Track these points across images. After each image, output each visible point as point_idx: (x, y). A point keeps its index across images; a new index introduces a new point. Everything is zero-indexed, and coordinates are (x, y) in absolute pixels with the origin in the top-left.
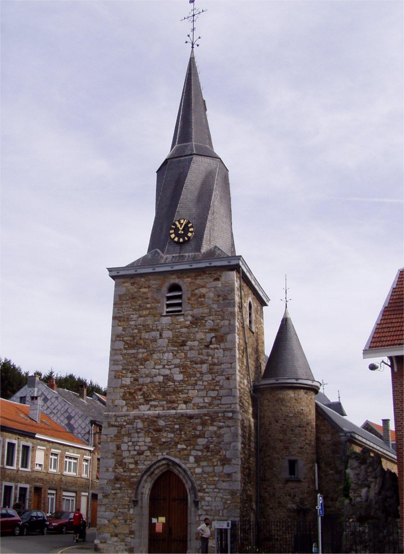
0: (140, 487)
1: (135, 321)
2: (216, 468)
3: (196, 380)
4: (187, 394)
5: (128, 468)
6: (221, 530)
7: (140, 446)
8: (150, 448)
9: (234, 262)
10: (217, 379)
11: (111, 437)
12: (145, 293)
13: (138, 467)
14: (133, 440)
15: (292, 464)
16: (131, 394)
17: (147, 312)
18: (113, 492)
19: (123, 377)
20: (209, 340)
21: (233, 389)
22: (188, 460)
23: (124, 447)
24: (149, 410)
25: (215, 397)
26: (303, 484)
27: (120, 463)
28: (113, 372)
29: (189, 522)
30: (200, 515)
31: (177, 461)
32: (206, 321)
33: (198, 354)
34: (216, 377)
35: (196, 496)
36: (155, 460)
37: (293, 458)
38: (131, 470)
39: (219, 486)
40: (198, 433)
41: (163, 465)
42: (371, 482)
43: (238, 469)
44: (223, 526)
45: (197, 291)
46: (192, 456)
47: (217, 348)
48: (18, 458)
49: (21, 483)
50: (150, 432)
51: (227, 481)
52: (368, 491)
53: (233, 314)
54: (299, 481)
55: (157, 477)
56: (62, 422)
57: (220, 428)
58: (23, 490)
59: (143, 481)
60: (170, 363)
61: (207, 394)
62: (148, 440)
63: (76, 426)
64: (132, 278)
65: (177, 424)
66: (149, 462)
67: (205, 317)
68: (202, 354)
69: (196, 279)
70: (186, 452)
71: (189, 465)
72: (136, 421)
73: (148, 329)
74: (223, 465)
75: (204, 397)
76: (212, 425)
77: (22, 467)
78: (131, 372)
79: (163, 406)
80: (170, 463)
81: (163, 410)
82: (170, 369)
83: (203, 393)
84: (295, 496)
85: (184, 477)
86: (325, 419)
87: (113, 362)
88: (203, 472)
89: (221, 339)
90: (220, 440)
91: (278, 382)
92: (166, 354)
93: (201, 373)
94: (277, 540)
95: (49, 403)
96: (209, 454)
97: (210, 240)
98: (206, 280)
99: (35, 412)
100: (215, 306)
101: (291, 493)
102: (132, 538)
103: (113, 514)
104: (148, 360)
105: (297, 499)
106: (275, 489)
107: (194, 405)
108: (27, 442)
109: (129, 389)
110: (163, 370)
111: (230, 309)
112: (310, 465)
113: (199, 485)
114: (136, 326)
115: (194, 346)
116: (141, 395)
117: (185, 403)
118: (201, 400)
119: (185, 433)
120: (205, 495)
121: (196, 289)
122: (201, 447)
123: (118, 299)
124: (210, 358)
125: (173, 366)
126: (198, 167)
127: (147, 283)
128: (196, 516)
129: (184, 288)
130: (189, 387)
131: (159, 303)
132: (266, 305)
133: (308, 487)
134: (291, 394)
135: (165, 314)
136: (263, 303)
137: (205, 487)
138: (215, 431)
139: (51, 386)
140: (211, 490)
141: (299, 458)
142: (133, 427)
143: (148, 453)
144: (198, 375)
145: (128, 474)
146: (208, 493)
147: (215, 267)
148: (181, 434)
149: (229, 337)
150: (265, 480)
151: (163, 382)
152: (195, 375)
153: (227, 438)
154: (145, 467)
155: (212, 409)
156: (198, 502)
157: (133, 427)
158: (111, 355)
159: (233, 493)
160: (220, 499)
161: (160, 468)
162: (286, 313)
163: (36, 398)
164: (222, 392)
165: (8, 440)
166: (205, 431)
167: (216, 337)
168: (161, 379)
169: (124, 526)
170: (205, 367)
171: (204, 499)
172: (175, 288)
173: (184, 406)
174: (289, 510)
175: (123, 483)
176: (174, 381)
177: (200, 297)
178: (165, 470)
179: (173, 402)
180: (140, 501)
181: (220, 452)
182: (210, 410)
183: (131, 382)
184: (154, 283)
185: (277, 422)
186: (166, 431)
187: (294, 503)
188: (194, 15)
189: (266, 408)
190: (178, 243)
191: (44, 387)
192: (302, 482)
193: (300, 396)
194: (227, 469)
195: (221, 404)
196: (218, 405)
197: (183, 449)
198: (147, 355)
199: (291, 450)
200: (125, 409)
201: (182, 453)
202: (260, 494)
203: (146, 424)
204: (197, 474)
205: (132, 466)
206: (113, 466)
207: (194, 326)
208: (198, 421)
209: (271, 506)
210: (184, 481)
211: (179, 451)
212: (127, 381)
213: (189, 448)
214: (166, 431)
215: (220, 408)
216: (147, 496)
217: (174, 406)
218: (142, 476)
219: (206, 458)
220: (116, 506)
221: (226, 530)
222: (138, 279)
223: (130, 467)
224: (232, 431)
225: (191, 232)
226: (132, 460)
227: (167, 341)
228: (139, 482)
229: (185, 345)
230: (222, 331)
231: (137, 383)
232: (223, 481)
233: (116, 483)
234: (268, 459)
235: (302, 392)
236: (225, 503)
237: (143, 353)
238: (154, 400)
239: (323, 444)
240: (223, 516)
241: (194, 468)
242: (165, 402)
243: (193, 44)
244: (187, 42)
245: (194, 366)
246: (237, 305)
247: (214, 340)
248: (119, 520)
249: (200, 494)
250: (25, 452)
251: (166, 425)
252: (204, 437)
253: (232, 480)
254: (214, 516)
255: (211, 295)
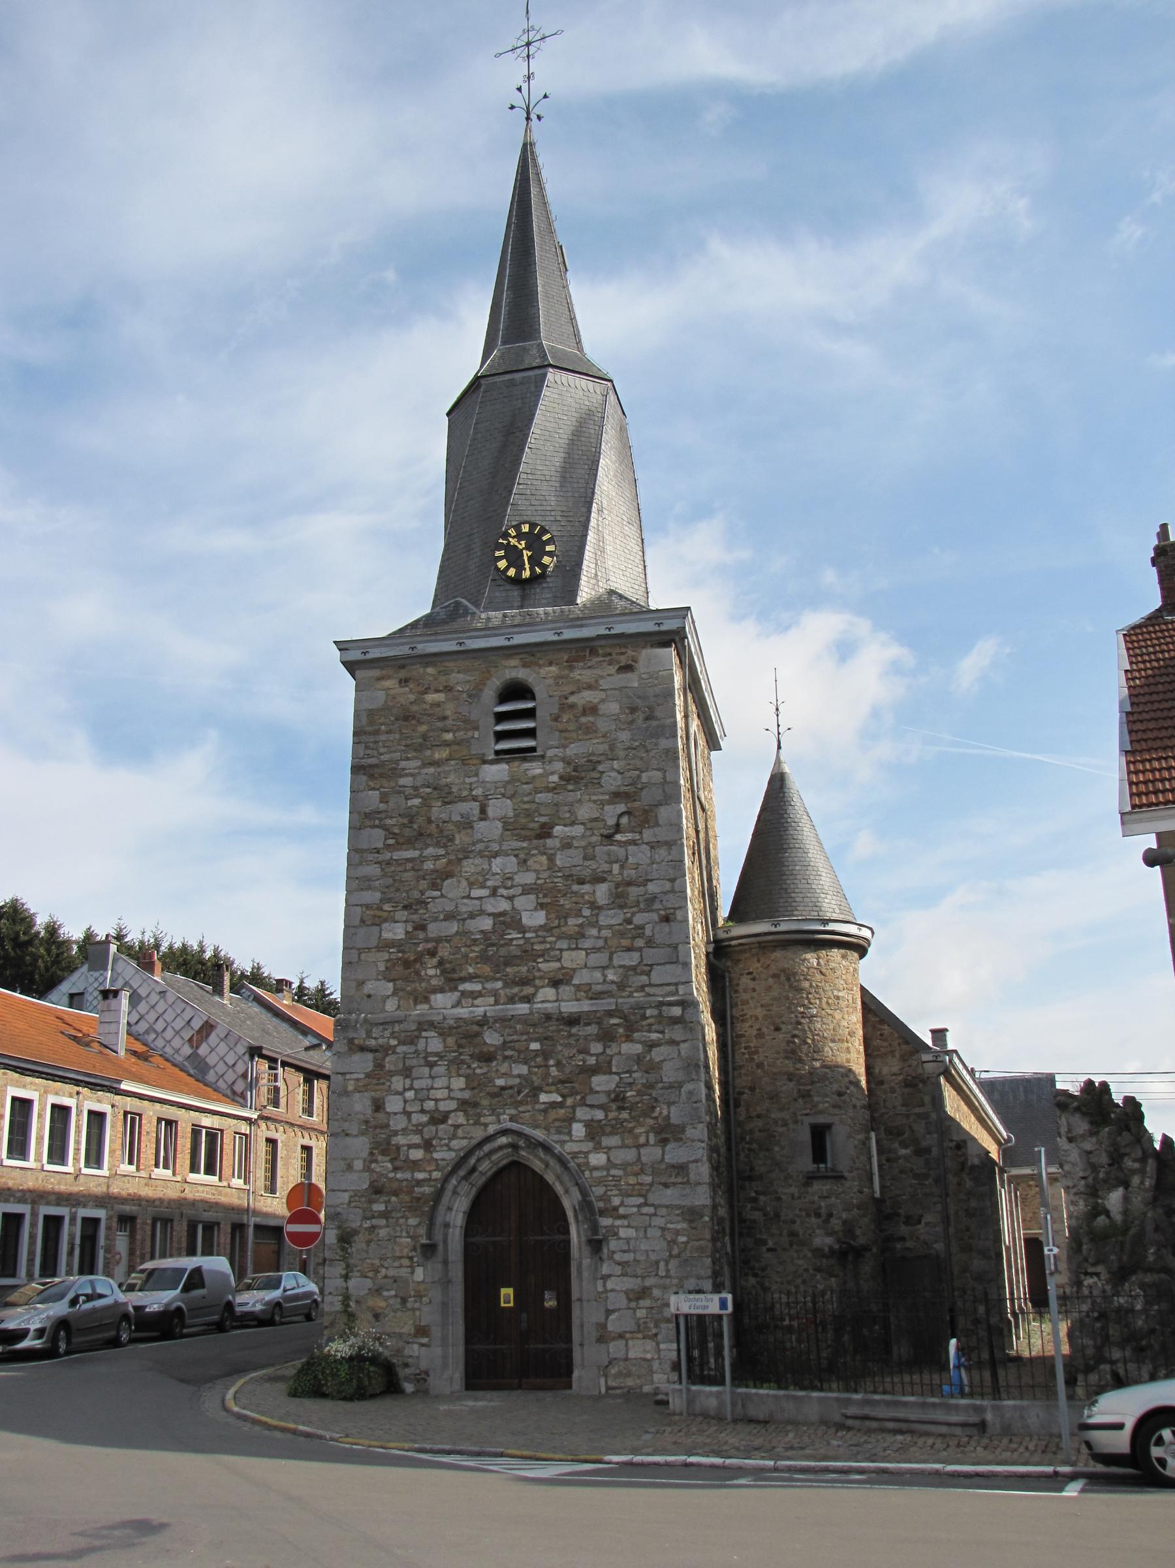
0: (442, 1208)
1: (412, 775)
2: (642, 1151)
3: (581, 926)
4: (559, 960)
5: (407, 1160)
6: (701, 1318)
7: (436, 1100)
8: (465, 1105)
9: (669, 625)
10: (638, 919)
11: (358, 1080)
12: (438, 705)
13: (435, 1155)
14: (417, 1084)
15: (819, 1133)
16: (407, 964)
17: (443, 753)
18: (367, 1224)
19: (386, 920)
20: (611, 822)
21: (680, 947)
22: (570, 1133)
23: (393, 1104)
24: (458, 1004)
25: (633, 968)
26: (848, 1184)
27: (385, 1147)
28: (359, 909)
29: (575, 1295)
30: (605, 1278)
31: (539, 1134)
32: (602, 773)
33: (585, 858)
34: (633, 914)
35: (595, 1228)
36: (479, 1134)
37: (821, 1119)
38: (415, 1165)
39: (652, 1198)
40: (592, 1061)
41: (501, 1148)
42: (1133, 1172)
43: (700, 1151)
44: (706, 1307)
45: (572, 699)
46: (580, 1121)
47: (633, 842)
48: (78, 1142)
49: (85, 1206)
50: (463, 1062)
51: (674, 1184)
52: (1126, 1199)
53: (672, 755)
54: (839, 1178)
55: (484, 1179)
56: (177, 1051)
57: (651, 1046)
58: (91, 1224)
59: (448, 1193)
60: (509, 883)
61: (611, 959)
62: (459, 1083)
63: (212, 1060)
64: (403, 667)
65: (536, 1040)
66: (464, 1142)
67: (599, 762)
68: (593, 858)
69: (571, 668)
70: (562, 1111)
71: (570, 1147)
72: (424, 1034)
73: (448, 797)
74: (664, 1142)
75: (604, 968)
76: (629, 1039)
77: (87, 1165)
78: (405, 907)
79: (495, 994)
80: (522, 1143)
81: (497, 1003)
82: (511, 898)
83: (601, 958)
84: (830, 1215)
85: (558, 1177)
86: (882, 1022)
87: (356, 883)
88: (610, 1164)
89: (645, 818)
90: (652, 1077)
91: (779, 929)
92: (499, 860)
93: (593, 906)
94: (790, 1329)
95: (143, 1007)
96: (625, 1115)
97: (596, 575)
98: (599, 672)
99: (113, 1027)
100: (624, 736)
101: (820, 1207)
102: (423, 1345)
103: (368, 1283)
104: (449, 875)
105: (835, 1223)
106: (779, 1199)
107: (578, 988)
108: (99, 1101)
109: (403, 952)
110: (492, 900)
111: (664, 743)
112: (861, 1137)
113: (600, 1199)
114: (416, 788)
115: (573, 838)
116: (436, 967)
117: (556, 983)
118: (598, 975)
119: (558, 1064)
120: (618, 1222)
121: (572, 693)
122: (603, 1099)
123: (364, 721)
124: (616, 867)
125: (520, 890)
126: (559, 400)
127: (442, 678)
128: (595, 1279)
129: (537, 690)
130: (563, 944)
131: (477, 728)
132: (718, 747)
133: (861, 1192)
134: (811, 958)
135: (492, 757)
136: (713, 743)
137: (616, 1201)
138: (638, 1055)
139: (148, 966)
140: (635, 1210)
141: (836, 1119)
142: (416, 1052)
143: (461, 1119)
144: (587, 912)
145: (408, 1175)
146: (624, 1217)
147: (622, 636)
148: (547, 1066)
149: (663, 813)
150: (750, 1178)
151: (494, 931)
152: (579, 914)
153: (670, 1073)
154: (453, 1154)
155: (625, 1002)
156: (600, 1242)
157: (416, 1052)
158: (350, 864)
159: (691, 1214)
160: (659, 1233)
161: (494, 1157)
162: (778, 762)
163: (116, 993)
164: (651, 955)
165: (52, 1099)
166: (612, 1056)
167: (628, 813)
168: (486, 924)
169: (399, 1314)
170: (602, 892)
171: (616, 1234)
172: (516, 691)
173: (548, 993)
174: (818, 1252)
175: (394, 1199)
176: (523, 930)
177: (584, 713)
178: (504, 1162)
179: (524, 982)
180: (441, 1248)
181: (653, 1108)
182: (620, 1000)
183: (407, 933)
184: (460, 679)
185: (777, 1029)
186: (506, 1058)
187: (829, 1234)
188: (528, 44)
189: (745, 996)
190: (517, 581)
191: (129, 968)
192: (846, 1179)
193: (832, 965)
194: (675, 1154)
195: (650, 985)
196: (642, 988)
197: (554, 1105)
198: (450, 862)
199: (816, 1099)
200: (391, 1005)
201: (553, 1114)
202: (740, 1213)
203: (451, 1041)
204: (596, 1168)
205: (417, 1154)
206: (365, 1154)
207: (570, 787)
208: (593, 1029)
209: (770, 1244)
210: (559, 1189)
211: (545, 1111)
212: (396, 931)
213: (569, 1101)
214: (506, 1058)
215: (649, 995)
216: (458, 1231)
217: (524, 993)
218: (446, 1179)
219: (616, 1128)
220: (377, 1262)
221: (719, 1317)
222: (418, 670)
223: (412, 1157)
224: (683, 1053)
225: (550, 554)
226: (416, 1139)
227: (500, 825)
228: (438, 1195)
229: (549, 835)
230: (646, 798)
231: (421, 935)
232: (666, 1185)
233: (375, 1202)
234: (759, 1123)
235: (836, 953)
236: (674, 1242)
237: (437, 858)
238: (470, 978)
239: (882, 1083)
240: (667, 1276)
241: (587, 1154)
242: (499, 984)
243: (528, 113)
244: (512, 107)
245: (575, 887)
246: (680, 733)
247: (624, 820)
248: (386, 1299)
249: (605, 1222)
250: (95, 1131)
251: (505, 1042)
252: (611, 1073)
253: (688, 1182)
254: (643, 1278)
255: (613, 707)
